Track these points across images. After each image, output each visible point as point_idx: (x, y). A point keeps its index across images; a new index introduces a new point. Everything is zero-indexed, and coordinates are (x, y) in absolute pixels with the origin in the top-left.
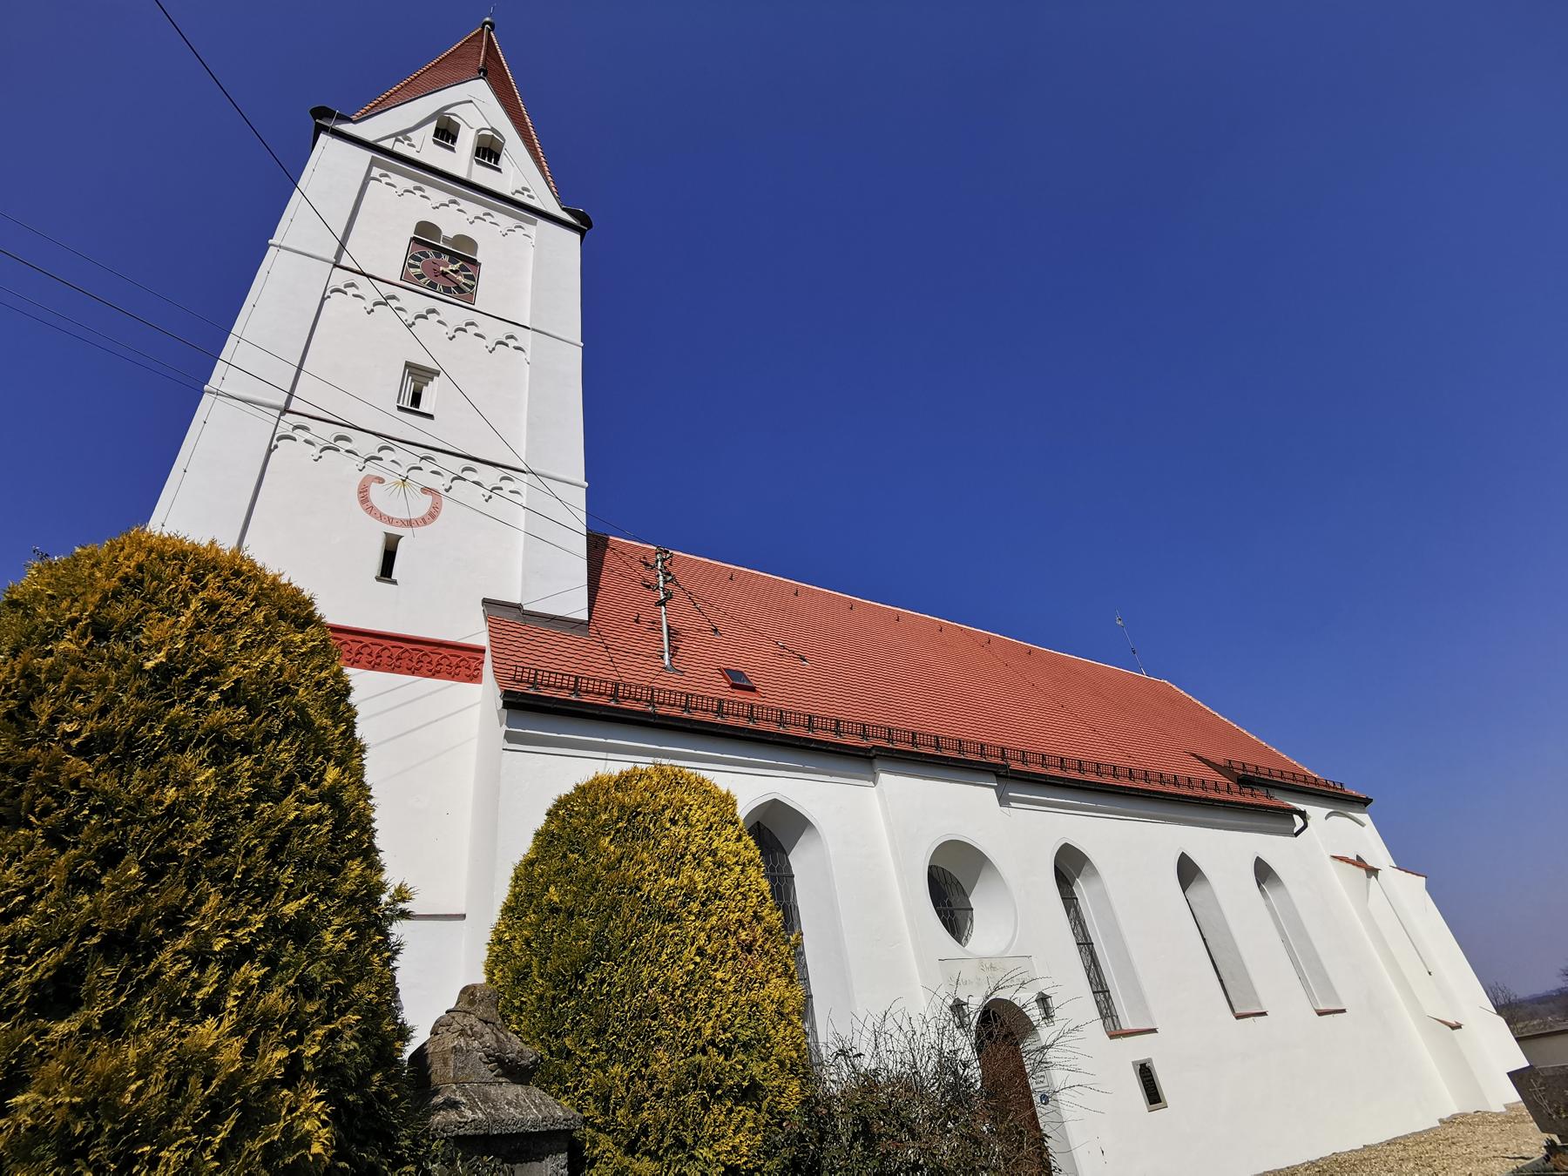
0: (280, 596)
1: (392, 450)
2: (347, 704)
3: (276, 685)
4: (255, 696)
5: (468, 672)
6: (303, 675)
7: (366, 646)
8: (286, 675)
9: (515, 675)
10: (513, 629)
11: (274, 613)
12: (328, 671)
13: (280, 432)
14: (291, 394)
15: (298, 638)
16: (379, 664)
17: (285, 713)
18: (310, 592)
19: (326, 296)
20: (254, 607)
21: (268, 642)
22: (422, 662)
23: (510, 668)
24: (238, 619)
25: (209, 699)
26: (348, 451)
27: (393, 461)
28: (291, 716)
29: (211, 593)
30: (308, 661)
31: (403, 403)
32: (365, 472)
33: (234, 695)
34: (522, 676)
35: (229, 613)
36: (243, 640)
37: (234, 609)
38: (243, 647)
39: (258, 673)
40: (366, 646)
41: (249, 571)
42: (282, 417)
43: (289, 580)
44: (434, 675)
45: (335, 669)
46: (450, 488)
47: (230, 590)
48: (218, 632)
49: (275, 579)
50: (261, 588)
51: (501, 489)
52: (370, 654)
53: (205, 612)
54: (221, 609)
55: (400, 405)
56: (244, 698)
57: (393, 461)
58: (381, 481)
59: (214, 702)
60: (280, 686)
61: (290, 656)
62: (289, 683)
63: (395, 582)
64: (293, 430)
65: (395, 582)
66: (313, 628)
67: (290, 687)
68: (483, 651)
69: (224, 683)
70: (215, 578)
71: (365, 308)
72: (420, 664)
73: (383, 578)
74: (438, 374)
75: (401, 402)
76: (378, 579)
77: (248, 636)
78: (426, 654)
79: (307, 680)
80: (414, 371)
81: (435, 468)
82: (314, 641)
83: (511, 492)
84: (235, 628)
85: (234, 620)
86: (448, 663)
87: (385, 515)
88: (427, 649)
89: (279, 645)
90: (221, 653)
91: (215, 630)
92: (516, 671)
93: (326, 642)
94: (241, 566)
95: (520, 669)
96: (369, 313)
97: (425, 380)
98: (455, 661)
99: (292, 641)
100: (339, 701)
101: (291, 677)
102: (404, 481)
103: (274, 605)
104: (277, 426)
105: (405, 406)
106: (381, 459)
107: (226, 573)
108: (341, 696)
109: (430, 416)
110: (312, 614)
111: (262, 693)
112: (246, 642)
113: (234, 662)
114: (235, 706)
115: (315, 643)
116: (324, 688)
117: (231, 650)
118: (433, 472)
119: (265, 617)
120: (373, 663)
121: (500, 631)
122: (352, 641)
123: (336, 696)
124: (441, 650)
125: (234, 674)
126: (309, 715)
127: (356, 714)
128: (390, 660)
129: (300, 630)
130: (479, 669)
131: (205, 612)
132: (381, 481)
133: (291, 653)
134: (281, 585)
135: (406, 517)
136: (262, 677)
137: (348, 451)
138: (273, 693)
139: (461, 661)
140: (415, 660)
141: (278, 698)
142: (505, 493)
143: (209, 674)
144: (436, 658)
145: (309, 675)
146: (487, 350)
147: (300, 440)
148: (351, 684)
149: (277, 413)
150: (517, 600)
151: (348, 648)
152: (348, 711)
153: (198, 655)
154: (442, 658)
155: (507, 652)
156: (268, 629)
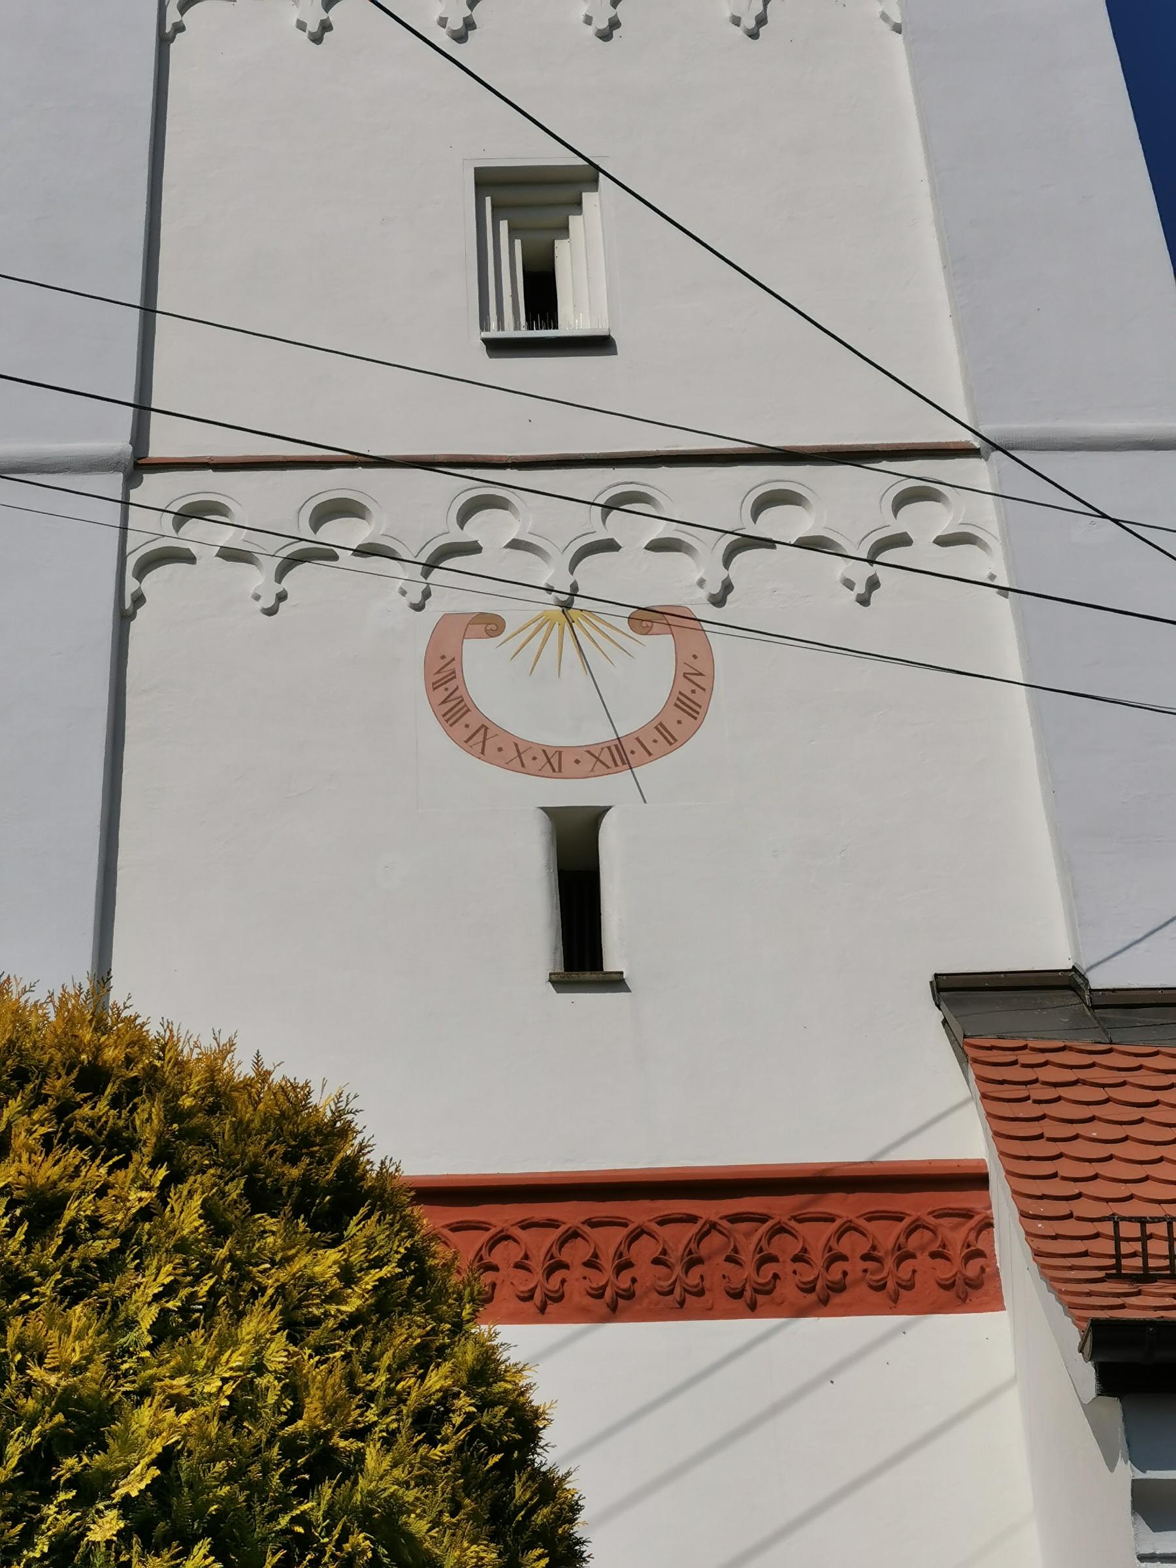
0: (242, 1130)
1: (501, 504)
2: (536, 1473)
3: (291, 1448)
4: (231, 1499)
5: (945, 1271)
6: (371, 1396)
7: (574, 1234)
8: (313, 1408)
9: (1118, 1256)
10: (1070, 1075)
11: (234, 1190)
12: (446, 1367)
13: (139, 546)
14: (143, 408)
15: (326, 1264)
16: (629, 1295)
17: (339, 1545)
18: (332, 1090)
19: (168, 29)
20: (166, 1183)
21: (236, 1298)
22: (773, 1259)
23: (1089, 1229)
24: (126, 1237)
25: (92, 1537)
26: (364, 551)
27: (515, 544)
28: (357, 1553)
29: (26, 1167)
30: (375, 1341)
31: (501, 326)
32: (436, 608)
33: (165, 1509)
34: (1145, 1255)
35: (95, 1224)
36: (154, 1310)
37: (105, 1205)
38: (162, 1331)
39: (224, 1417)
40: (574, 1234)
41: (129, 1061)
42: (135, 495)
43: (258, 1062)
44: (825, 1301)
45: (468, 1354)
46: (728, 587)
47: (82, 1141)
48: (71, 1295)
49: (213, 1071)
50: (174, 1114)
51: (903, 540)
52: (592, 1263)
53: (20, 1235)
54: (68, 1215)
55: (494, 333)
56: (199, 1512)
57: (515, 544)
58: (491, 625)
59: (109, 1543)
60: (301, 1451)
61: (315, 1336)
62: (328, 1435)
63: (616, 983)
64: (178, 527)
65: (616, 983)
66: (367, 1216)
67: (335, 1450)
68: (977, 1180)
69: (127, 1471)
70: (29, 1109)
71: (301, 26)
72: (770, 1269)
73: (575, 976)
74: (593, 184)
75: (494, 324)
76: (560, 983)
77: (169, 1291)
78: (779, 1229)
79: (385, 1412)
80: (509, 195)
81: (660, 530)
82: (378, 1263)
83: (943, 541)
84: (122, 1269)
85: (116, 1243)
86: (865, 1248)
87: (531, 745)
88: (780, 1207)
89: (272, 1304)
90: (97, 1370)
91: (65, 1292)
92: (1117, 1239)
93: (421, 1261)
94: (99, 1049)
95: (1130, 1230)
96: (317, 39)
97: (550, 217)
98: (887, 1235)
99: (311, 1282)
100: (506, 1470)
101: (330, 1412)
102: (566, 606)
103: (228, 1164)
104: (124, 528)
105: (509, 332)
106: (473, 548)
107: (56, 1085)
108: (508, 1448)
109: (600, 344)
110: (351, 1166)
111: (249, 1486)
112: (164, 1313)
113: (144, 1393)
114: (176, 1547)
115: (385, 1272)
116: (447, 1430)
117: (126, 1352)
118: (658, 546)
119: (208, 1213)
120: (608, 1293)
121: (1021, 1092)
122: (526, 1225)
123: (493, 1450)
124: (833, 1203)
125: (152, 1434)
126: (410, 1537)
127: (575, 1508)
128: (871, 1265)
129: (329, 1237)
130: (980, 1254)
131: (20, 1235)
132: (491, 625)
133: (315, 1322)
134: (235, 1088)
135: (602, 734)
136: (238, 1426)
137: (364, 551)
138: (286, 1479)
139: (910, 1231)
140: (748, 1256)
141: (304, 1492)
142: (923, 553)
143: (75, 1447)
144: (817, 1236)
145: (390, 1392)
146: (739, 32)
147: (206, 555)
148: (537, 1399)
149: (112, 484)
150: (1059, 958)
151: (654, 1250)
152: (543, 1502)
153: (28, 1388)
154: (840, 1234)
155: (1066, 1168)
156: (222, 1253)
